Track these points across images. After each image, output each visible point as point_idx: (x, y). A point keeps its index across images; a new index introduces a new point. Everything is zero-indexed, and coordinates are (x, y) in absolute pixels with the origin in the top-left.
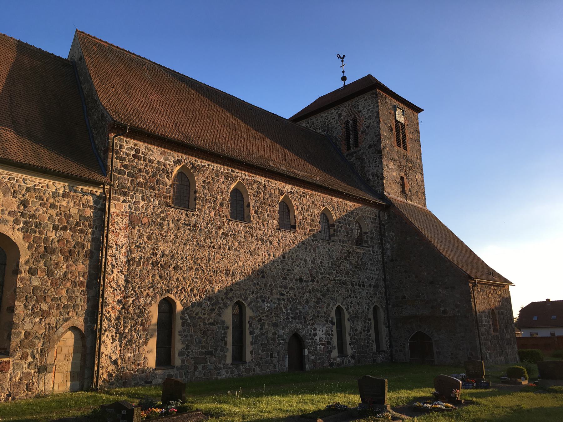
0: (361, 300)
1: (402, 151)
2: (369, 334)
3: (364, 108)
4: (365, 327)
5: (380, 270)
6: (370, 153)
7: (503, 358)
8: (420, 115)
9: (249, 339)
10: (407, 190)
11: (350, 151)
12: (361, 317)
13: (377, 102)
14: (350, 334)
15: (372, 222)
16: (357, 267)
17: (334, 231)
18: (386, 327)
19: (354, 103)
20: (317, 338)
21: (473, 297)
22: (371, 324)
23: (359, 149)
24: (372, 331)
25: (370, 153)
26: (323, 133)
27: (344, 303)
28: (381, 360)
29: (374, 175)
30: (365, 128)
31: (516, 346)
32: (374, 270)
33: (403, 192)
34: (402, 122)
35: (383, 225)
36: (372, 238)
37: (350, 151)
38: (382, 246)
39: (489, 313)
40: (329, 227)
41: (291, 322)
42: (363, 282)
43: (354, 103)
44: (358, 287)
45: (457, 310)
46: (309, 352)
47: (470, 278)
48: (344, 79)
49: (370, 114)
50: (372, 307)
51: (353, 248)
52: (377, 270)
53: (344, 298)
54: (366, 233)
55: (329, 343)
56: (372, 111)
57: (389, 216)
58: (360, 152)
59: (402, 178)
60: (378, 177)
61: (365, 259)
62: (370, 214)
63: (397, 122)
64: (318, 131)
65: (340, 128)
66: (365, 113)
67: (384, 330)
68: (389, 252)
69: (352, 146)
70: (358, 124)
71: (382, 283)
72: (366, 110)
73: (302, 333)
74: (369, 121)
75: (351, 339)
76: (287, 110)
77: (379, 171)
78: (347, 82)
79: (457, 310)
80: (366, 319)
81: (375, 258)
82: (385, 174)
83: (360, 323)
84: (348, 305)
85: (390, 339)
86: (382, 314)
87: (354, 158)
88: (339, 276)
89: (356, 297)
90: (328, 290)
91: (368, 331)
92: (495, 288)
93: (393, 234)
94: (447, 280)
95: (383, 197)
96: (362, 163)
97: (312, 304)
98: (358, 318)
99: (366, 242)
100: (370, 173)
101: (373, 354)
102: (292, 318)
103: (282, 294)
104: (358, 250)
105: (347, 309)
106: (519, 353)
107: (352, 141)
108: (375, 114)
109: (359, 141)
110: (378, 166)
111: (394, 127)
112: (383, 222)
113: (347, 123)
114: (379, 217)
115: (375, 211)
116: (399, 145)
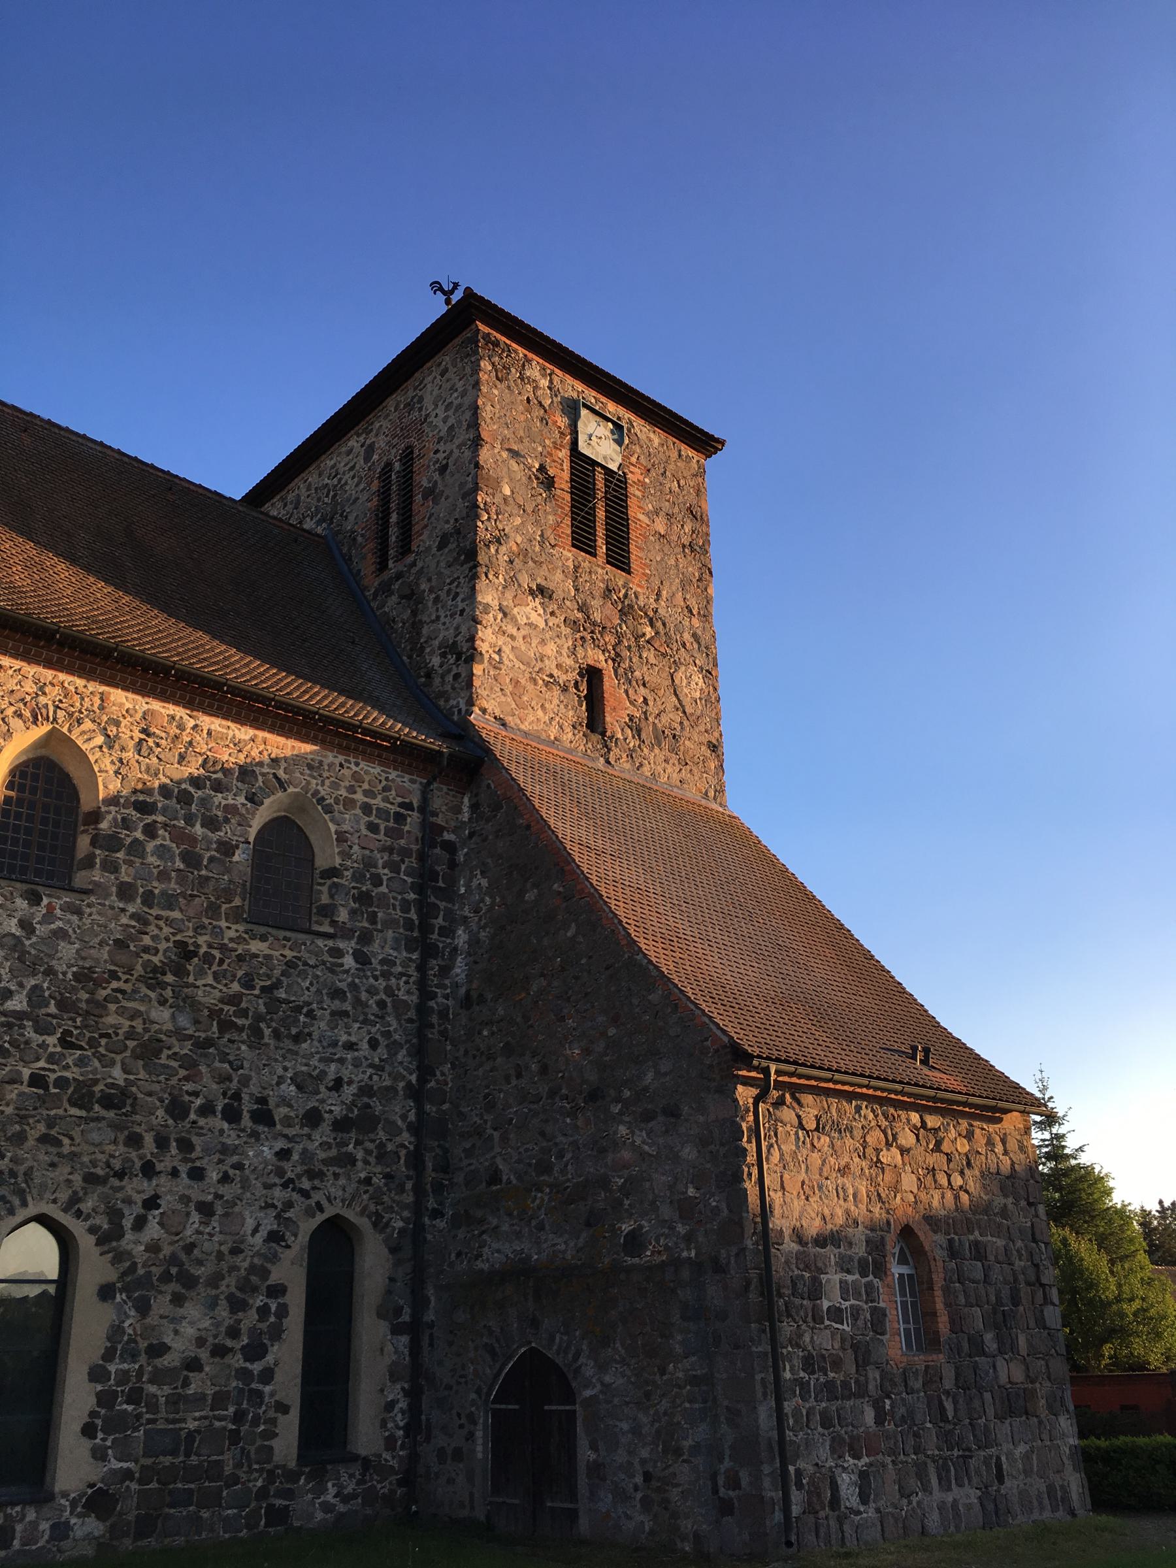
0: (228, 1191)
1: (599, 571)
2: (256, 1367)
4: (234, 1332)
5: (393, 1047)
6: (443, 564)
7: (967, 1495)
8: (711, 463)
10: (614, 721)
11: (386, 576)
12: (215, 1280)
13: (476, 369)
14: (97, 1374)
15: (373, 828)
16: (226, 1026)
18: (396, 1330)
19: (411, 393)
21: (751, 1158)
22: (283, 1311)
24: (287, 1356)
26: (319, 530)
27: (87, 1206)
28: (327, 1508)
30: (436, 476)
31: (1066, 1424)
32: (350, 1046)
33: (594, 721)
35: (450, 847)
36: (364, 898)
38: (424, 944)
39: (876, 1246)
42: (263, 1101)
43: (411, 393)
44: (218, 1123)
45: (681, 1229)
47: (742, 1057)
50: (307, 1227)
51: (217, 932)
52: (373, 1044)
53: (91, 1179)
54: (332, 872)
57: (474, 807)
58: (414, 570)
59: (592, 675)
61: (303, 989)
62: (368, 793)
64: (308, 525)
66: (437, 421)
67: (375, 1345)
68: (460, 968)
69: (392, 552)
71: (400, 1110)
72: (440, 411)
74: (449, 447)
75: (105, 1399)
76: (231, 468)
77: (463, 629)
79: (681, 1229)
80: (246, 1286)
81: (372, 991)
82: (487, 639)
83: (192, 1310)
84: (115, 1215)
85: (414, 1394)
86: (374, 1265)
87: (395, 598)
88: (81, 1062)
89: (197, 1174)
91: (255, 1351)
92: (932, 1121)
94: (650, 1076)
95: (462, 732)
98: (190, 1282)
99: (327, 912)
100: (436, 643)
101: (271, 1476)
104: (256, 946)
106: (1087, 1459)
108: (468, 415)
110: (462, 611)
111: (563, 476)
112: (447, 836)
115: (407, 784)
116: (583, 541)
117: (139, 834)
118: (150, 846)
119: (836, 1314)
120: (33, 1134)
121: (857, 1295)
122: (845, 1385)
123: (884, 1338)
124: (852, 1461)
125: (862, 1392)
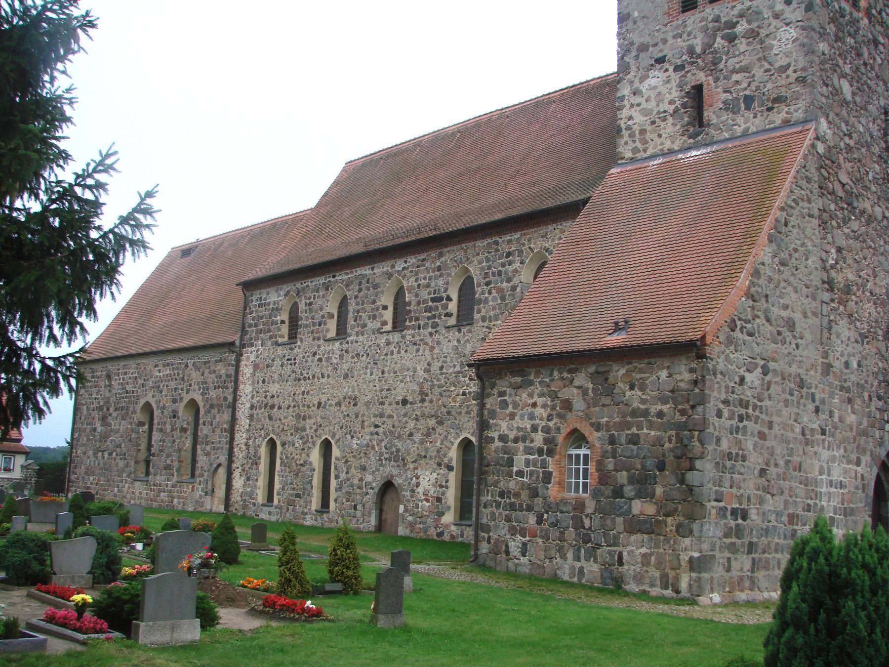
97: (417, 437)
117: (486, 295)
118: (490, 298)
119: (520, 473)
120: (463, 412)
121: (535, 465)
122: (521, 505)
123: (549, 486)
124: (520, 537)
125: (530, 508)
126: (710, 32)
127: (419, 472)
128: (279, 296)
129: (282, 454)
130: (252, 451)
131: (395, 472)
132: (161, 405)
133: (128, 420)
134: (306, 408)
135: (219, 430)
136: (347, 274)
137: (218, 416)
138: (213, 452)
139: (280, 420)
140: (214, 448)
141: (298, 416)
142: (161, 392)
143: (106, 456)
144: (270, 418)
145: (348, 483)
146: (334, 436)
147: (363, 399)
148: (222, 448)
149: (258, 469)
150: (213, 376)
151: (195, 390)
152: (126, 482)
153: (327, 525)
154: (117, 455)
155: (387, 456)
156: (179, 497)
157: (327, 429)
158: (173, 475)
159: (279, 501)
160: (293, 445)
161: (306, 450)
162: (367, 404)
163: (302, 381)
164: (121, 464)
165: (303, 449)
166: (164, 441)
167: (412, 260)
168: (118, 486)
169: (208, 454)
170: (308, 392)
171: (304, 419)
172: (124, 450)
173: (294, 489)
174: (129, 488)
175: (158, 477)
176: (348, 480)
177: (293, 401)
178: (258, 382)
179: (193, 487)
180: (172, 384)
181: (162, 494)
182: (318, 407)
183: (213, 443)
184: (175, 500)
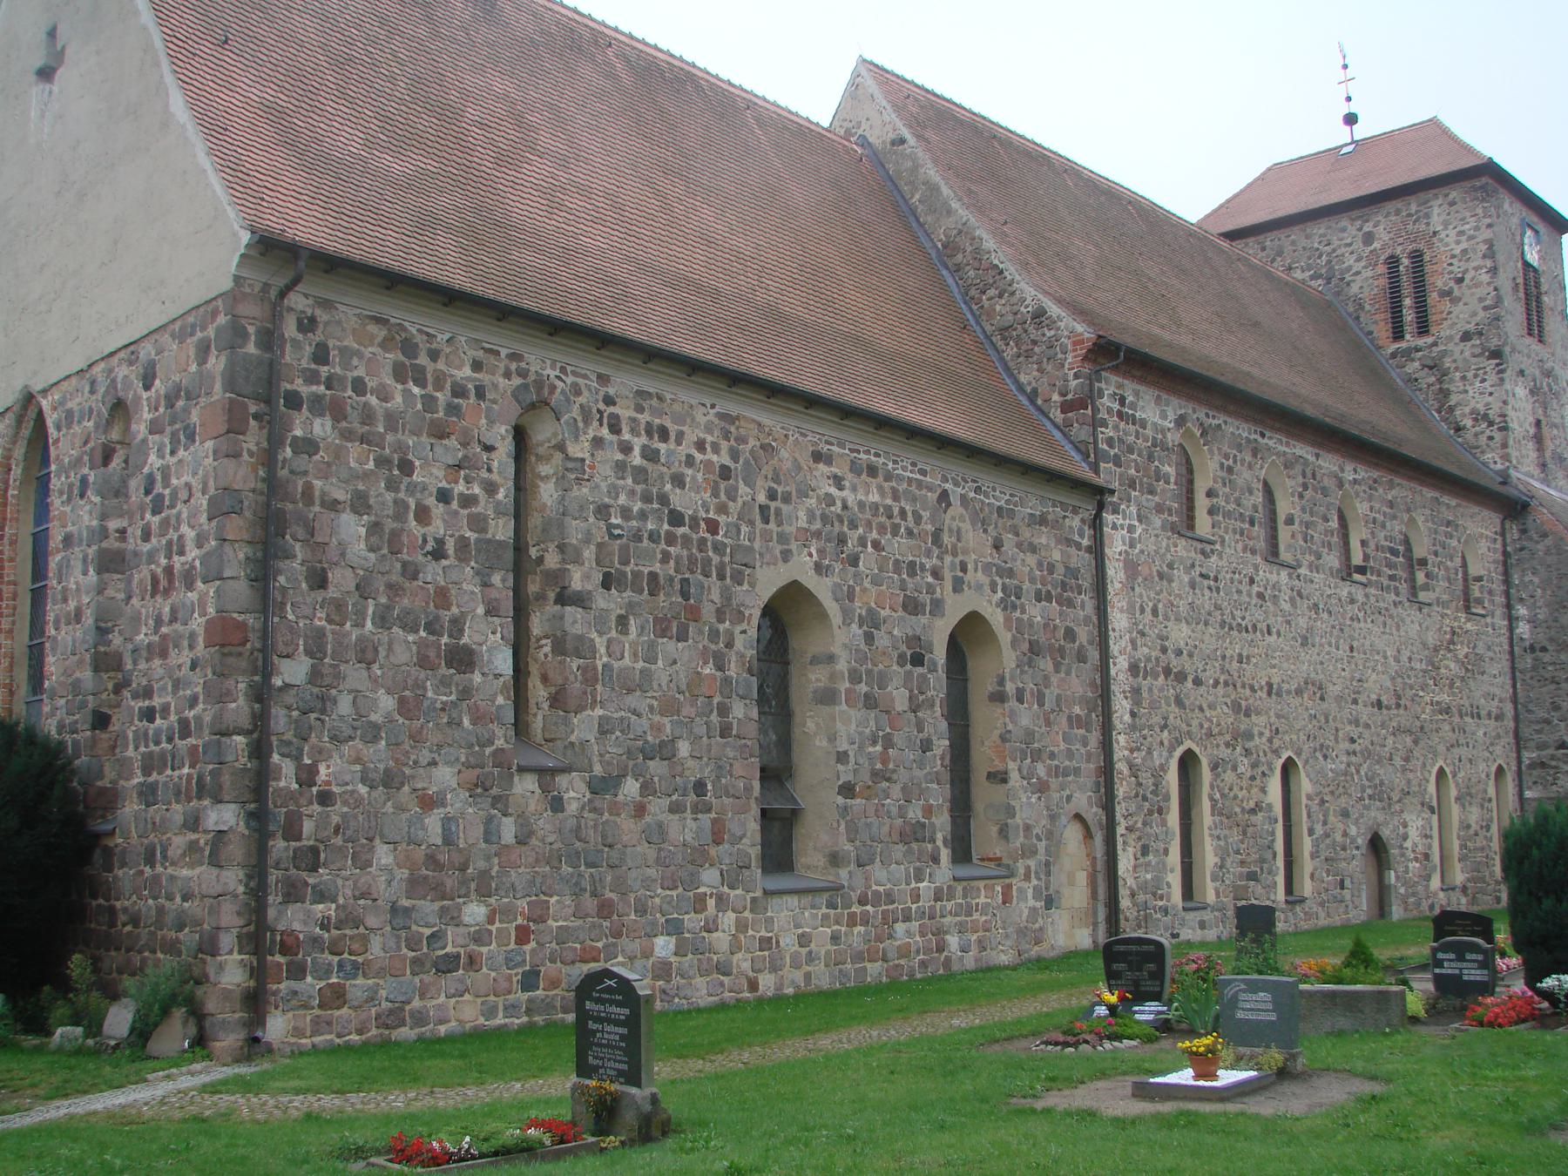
3: (1446, 225)
6: (1467, 354)
9: (1307, 844)
11: (1403, 345)
17: (1427, 575)
20: (1408, 844)
23: (1430, 340)
25: (1467, 354)
29: (1481, 417)
30: (1452, 284)
34: (1535, 264)
37: (1403, 345)
40: (1411, 566)
41: (1367, 808)
46: (1397, 878)
48: (1351, 120)
49: (1464, 245)
54: (1479, 579)
55: (1427, 856)
56: (1471, 238)
60: (1491, 424)
63: (1526, 265)
65: (1370, 274)
70: (1428, 268)
71: (1508, 708)
73: (1386, 833)
74: (1464, 265)
78: (1362, 131)
90: (1422, 728)
93: (1536, 580)
96: (1440, 381)
97: (1398, 762)
100: (1467, 410)
102: (1370, 797)
103: (1353, 741)
104: (1469, 626)
105: (1454, 776)
107: (1409, 316)
109: (1432, 318)
113: (1393, 262)
114: (1503, 534)
126: (273, 293)
127: (1406, 816)
128: (1164, 416)
129: (1212, 787)
130: (1148, 782)
131: (1381, 817)
132: (859, 607)
133: (698, 637)
134: (1248, 692)
135: (1064, 721)
136: (1280, 441)
137: (1054, 680)
138: (1054, 783)
139: (1201, 709)
140: (1057, 772)
141: (1236, 707)
142: (854, 561)
143: (574, 790)
144: (1179, 702)
145: (1328, 841)
146: (1299, 754)
147: (1333, 690)
148: (1077, 771)
149: (1164, 823)
150: (1031, 560)
151: (979, 587)
152: (721, 900)
153: (1305, 926)
154: (646, 788)
155: (1369, 791)
156: (962, 929)
157: (1287, 738)
158: (936, 859)
159: (1218, 895)
160: (1235, 768)
161: (1258, 778)
162: (1339, 699)
163: (1235, 633)
164: (686, 830)
165: (1253, 778)
166: (888, 743)
167: (1363, 473)
168: (674, 928)
169: (1042, 788)
170: (1248, 657)
171: (1247, 715)
172: (695, 770)
173: (1242, 863)
174: (742, 926)
175: (878, 871)
176: (1327, 836)
177: (1222, 670)
178: (1142, 611)
179: (1007, 890)
180: (898, 546)
181: (900, 928)
182: (1269, 694)
183: (1052, 756)
184: (953, 941)
